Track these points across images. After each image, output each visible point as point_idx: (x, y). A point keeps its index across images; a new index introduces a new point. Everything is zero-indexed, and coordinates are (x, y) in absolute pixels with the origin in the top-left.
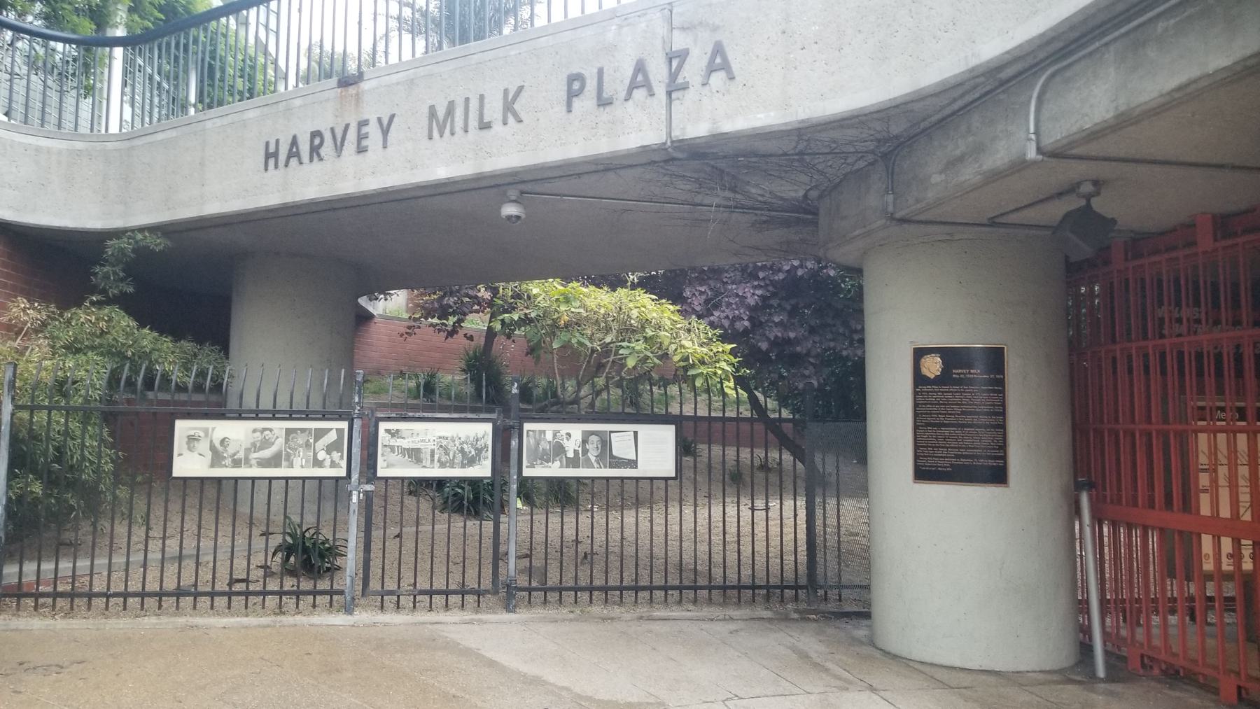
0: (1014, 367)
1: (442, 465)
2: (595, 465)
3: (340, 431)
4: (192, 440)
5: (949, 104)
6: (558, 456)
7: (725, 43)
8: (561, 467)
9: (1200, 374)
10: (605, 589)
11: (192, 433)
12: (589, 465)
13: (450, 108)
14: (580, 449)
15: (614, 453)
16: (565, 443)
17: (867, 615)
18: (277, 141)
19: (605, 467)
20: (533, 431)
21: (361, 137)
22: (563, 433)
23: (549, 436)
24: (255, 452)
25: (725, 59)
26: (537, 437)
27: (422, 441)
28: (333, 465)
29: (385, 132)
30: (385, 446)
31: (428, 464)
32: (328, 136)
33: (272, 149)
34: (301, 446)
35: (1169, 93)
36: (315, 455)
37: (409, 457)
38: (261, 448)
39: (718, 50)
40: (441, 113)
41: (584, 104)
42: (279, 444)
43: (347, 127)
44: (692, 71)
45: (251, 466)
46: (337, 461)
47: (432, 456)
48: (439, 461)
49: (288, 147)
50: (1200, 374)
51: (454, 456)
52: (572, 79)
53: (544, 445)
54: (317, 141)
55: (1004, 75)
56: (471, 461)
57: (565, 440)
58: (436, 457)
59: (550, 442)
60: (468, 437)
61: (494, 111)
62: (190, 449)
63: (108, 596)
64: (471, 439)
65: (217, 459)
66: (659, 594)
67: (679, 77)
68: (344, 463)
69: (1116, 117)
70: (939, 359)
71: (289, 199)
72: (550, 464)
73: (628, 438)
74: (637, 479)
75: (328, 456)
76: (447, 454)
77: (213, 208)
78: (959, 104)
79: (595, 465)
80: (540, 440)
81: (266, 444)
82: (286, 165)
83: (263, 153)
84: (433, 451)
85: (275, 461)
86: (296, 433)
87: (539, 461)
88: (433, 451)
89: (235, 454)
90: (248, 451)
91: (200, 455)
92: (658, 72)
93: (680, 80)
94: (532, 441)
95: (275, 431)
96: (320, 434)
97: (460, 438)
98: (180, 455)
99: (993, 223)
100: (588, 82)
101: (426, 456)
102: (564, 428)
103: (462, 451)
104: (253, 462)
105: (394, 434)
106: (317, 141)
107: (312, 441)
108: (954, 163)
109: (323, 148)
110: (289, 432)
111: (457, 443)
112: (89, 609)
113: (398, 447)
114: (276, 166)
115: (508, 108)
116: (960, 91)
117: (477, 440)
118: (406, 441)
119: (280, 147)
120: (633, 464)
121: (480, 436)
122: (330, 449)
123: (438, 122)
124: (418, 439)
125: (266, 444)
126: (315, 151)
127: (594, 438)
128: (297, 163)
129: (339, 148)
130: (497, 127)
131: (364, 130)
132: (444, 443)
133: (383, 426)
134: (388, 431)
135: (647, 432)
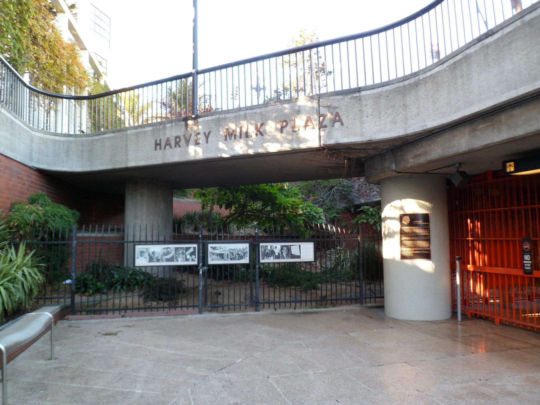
0: (432, 220)
1: (231, 259)
3: (194, 248)
4: (142, 253)
7: (340, 113)
8: (274, 259)
9: (506, 219)
11: (142, 250)
12: (283, 258)
15: (292, 253)
16: (275, 250)
22: (274, 246)
23: (269, 248)
28: (193, 260)
29: (207, 137)
31: (226, 259)
32: (182, 138)
34: (180, 254)
35: (484, 146)
36: (186, 257)
38: (167, 255)
42: (173, 253)
46: (194, 259)
47: (228, 256)
48: (230, 258)
49: (165, 142)
50: (506, 219)
51: (235, 256)
53: (267, 251)
54: (178, 140)
55: (434, 132)
56: (241, 258)
60: (240, 249)
62: (141, 256)
65: (151, 259)
68: (196, 260)
69: (469, 150)
74: (300, 262)
76: (233, 255)
81: (168, 253)
82: (165, 148)
83: (154, 143)
84: (228, 254)
85: (171, 260)
88: (228, 254)
90: (162, 256)
93: (324, 124)
94: (263, 250)
96: (188, 249)
99: (427, 173)
101: (225, 256)
102: (274, 245)
103: (238, 254)
104: (164, 260)
106: (178, 140)
107: (184, 252)
110: (176, 249)
111: (236, 251)
114: (160, 149)
116: (420, 135)
120: (299, 257)
122: (191, 254)
125: (168, 253)
126: (177, 144)
132: (232, 251)
133: (210, 246)
134: (211, 247)
135: (304, 245)
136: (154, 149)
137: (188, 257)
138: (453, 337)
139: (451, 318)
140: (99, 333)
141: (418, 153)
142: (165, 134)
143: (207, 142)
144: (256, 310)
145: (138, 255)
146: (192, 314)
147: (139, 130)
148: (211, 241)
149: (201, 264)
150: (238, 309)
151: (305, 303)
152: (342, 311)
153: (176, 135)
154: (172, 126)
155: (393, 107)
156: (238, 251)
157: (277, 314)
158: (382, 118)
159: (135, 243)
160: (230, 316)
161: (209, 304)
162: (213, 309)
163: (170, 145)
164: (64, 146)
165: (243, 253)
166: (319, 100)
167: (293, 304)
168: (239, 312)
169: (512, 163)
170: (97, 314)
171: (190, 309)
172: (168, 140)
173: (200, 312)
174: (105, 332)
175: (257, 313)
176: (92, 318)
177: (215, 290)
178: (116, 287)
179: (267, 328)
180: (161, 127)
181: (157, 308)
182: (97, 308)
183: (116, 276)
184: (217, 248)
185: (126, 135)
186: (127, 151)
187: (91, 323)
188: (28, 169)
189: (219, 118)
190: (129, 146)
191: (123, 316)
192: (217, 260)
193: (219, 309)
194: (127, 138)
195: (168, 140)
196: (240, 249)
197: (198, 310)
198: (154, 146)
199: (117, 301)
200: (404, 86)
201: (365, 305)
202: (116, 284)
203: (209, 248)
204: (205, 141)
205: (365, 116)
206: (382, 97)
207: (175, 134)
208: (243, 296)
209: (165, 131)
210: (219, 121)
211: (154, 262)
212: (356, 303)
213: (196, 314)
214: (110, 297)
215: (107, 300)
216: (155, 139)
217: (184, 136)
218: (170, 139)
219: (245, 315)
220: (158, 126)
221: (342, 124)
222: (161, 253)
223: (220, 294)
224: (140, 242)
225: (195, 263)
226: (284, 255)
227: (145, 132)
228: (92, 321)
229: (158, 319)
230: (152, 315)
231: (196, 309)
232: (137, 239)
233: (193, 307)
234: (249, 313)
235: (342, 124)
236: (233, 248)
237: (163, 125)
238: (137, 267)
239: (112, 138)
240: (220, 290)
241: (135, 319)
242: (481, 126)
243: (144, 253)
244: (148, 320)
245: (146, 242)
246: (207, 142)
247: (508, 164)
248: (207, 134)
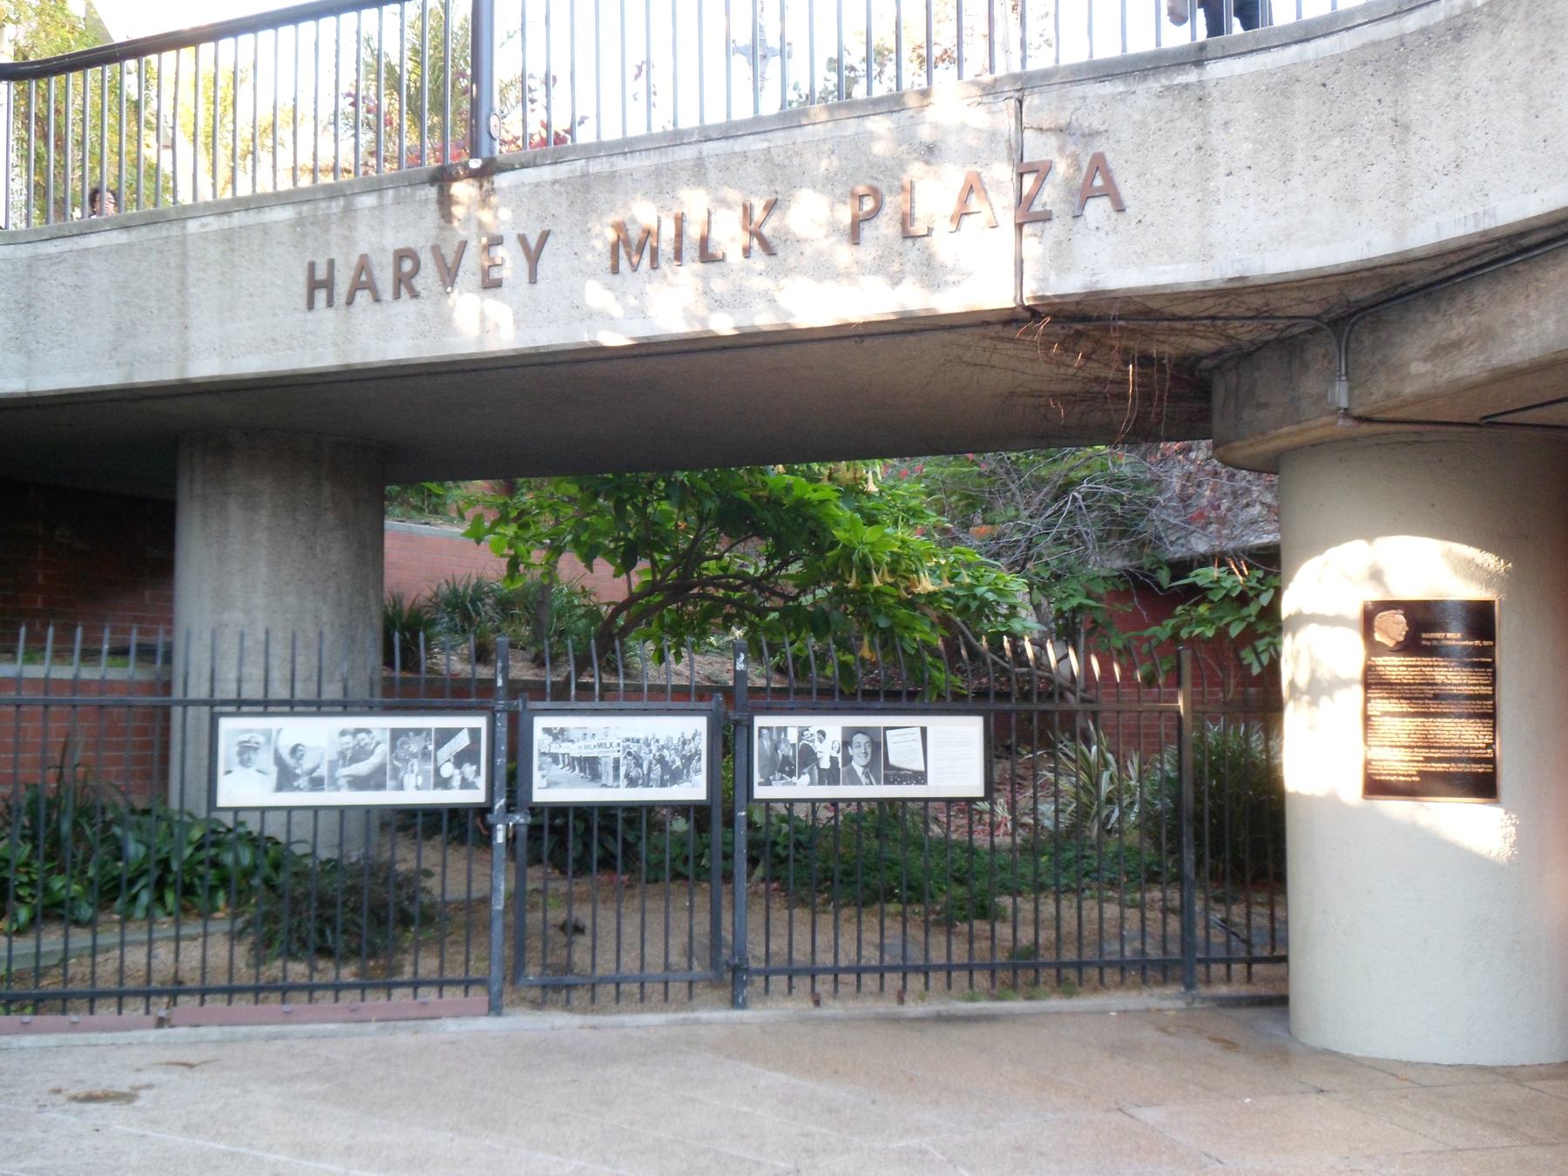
1: (632, 782)
2: (863, 779)
3: (474, 733)
4: (246, 751)
5: (1442, 269)
6: (806, 766)
7: (1109, 157)
8: (812, 783)
11: (245, 737)
12: (853, 779)
14: (840, 756)
15: (893, 761)
16: (817, 747)
18: (331, 263)
19: (878, 783)
20: (768, 728)
22: (814, 730)
23: (792, 736)
24: (344, 766)
25: (1109, 180)
26: (775, 736)
27: (600, 745)
28: (466, 784)
29: (533, 257)
30: (544, 754)
31: (610, 781)
32: (426, 259)
33: (321, 274)
34: (414, 756)
36: (437, 771)
37: (581, 771)
39: (1099, 164)
42: (381, 753)
43: (464, 245)
45: (338, 788)
47: (616, 768)
48: (627, 776)
49: (352, 273)
53: (784, 750)
54: (407, 266)
55: (1525, 242)
56: (673, 776)
57: (817, 743)
58: (622, 771)
59: (793, 746)
60: (670, 739)
62: (244, 763)
64: (675, 741)
65: (286, 779)
67: (1036, 202)
68: (481, 782)
70: (1402, 618)
72: (795, 779)
73: (913, 737)
74: (927, 800)
75: (457, 772)
77: (206, 367)
78: (1458, 269)
79: (863, 779)
80: (779, 742)
81: (359, 754)
82: (350, 301)
83: (301, 278)
84: (617, 761)
85: (374, 781)
86: (408, 736)
87: (778, 775)
88: (617, 761)
89: (314, 770)
90: (333, 766)
91: (260, 771)
94: (767, 744)
95: (375, 733)
96: (445, 736)
97: (657, 741)
98: (228, 772)
99: (1489, 422)
101: (606, 769)
102: (815, 723)
103: (661, 760)
104: (343, 782)
105: (557, 735)
106: (407, 266)
107: (431, 748)
108: (1443, 350)
109: (418, 278)
110: (396, 734)
111: (654, 748)
113: (564, 755)
114: (330, 303)
117: (684, 743)
118: (576, 745)
119: (336, 273)
120: (920, 777)
121: (688, 736)
122: (461, 759)
124: (595, 742)
125: (359, 754)
126: (404, 283)
127: (860, 739)
128: (370, 299)
129: (449, 274)
132: (634, 748)
133: (540, 723)
134: (547, 731)
136: (303, 302)
137: (447, 770)
140: (58, 1091)
142: (349, 241)
143: (533, 278)
144: (735, 1003)
145: (228, 761)
146: (457, 1016)
147: (239, 219)
148: (547, 704)
149: (500, 803)
152: (1104, 1012)
153: (401, 245)
154: (381, 206)
155: (1348, 129)
157: (822, 1021)
158: (1296, 182)
159: (217, 709)
160: (622, 1026)
161: (532, 972)
162: (550, 995)
163: (371, 286)
165: (683, 757)
166: (1021, 102)
167: (893, 980)
168: (662, 1010)
170: (50, 1010)
171: (453, 994)
172: (364, 265)
173: (495, 1009)
174: (80, 1090)
175: (737, 1014)
176: (25, 1029)
177: (557, 915)
178: (135, 898)
179: (781, 1077)
180: (336, 206)
181: (310, 989)
182: (49, 984)
183: (134, 849)
185: (183, 242)
186: (183, 312)
187: (21, 1049)
189: (585, 175)
190: (193, 290)
191: (161, 1023)
192: (572, 784)
193: (575, 994)
194: (185, 254)
195: (364, 265)
197: (486, 999)
198: (301, 289)
199: (136, 957)
200: (1401, 40)
201: (1203, 991)
202: (132, 882)
205: (1222, 170)
206: (1298, 87)
207: (394, 240)
208: (678, 941)
209: (351, 229)
210: (587, 188)
211: (298, 788)
212: (1165, 981)
213: (476, 1015)
214: (108, 937)
215: (94, 951)
216: (310, 259)
217: (436, 250)
218: (374, 260)
219: (685, 1022)
220: (322, 205)
222: (332, 754)
223: (579, 930)
224: (241, 706)
225: (478, 796)
226: (858, 766)
227: (265, 229)
228: (27, 1041)
229: (311, 1037)
230: (287, 1018)
231: (478, 996)
232: (227, 690)
233: (467, 984)
234: (704, 1015)
236: (641, 736)
237: (342, 202)
239: (119, 249)
240: (582, 913)
241: (214, 1032)
243: (256, 749)
244: (269, 1038)
245: (266, 706)
246: (533, 278)
248: (533, 242)
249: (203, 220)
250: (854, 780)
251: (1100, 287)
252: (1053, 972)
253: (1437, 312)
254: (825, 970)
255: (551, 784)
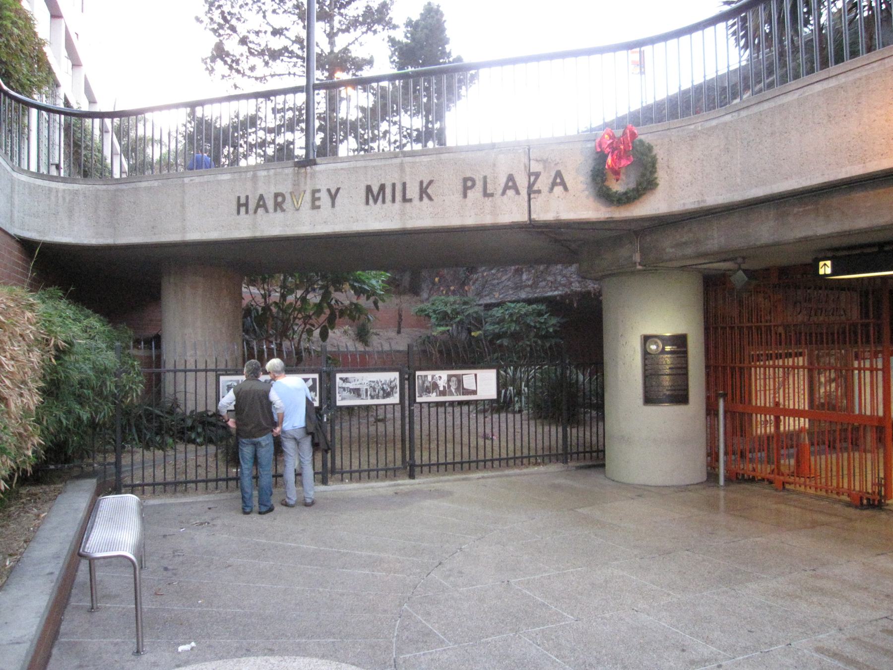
1: (372, 397)
3: (314, 380)
7: (563, 172)
8: (437, 396)
10: (438, 465)
11: (230, 383)
12: (451, 394)
13: (382, 188)
15: (465, 386)
17: (603, 466)
18: (247, 197)
21: (314, 199)
22: (437, 376)
23: (430, 379)
29: (333, 197)
32: (288, 196)
33: (243, 201)
39: (559, 174)
40: (375, 189)
41: (475, 194)
44: (543, 183)
47: (367, 392)
48: (370, 395)
52: (465, 180)
53: (427, 384)
56: (387, 395)
60: (386, 381)
61: (413, 192)
63: (469, 462)
66: (381, 473)
71: (258, 234)
74: (477, 401)
82: (255, 212)
83: (235, 203)
84: (367, 390)
92: (522, 182)
93: (535, 188)
94: (420, 382)
100: (477, 182)
101: (363, 393)
102: (438, 373)
103: (383, 389)
105: (345, 380)
106: (280, 199)
111: (380, 384)
112: (446, 470)
114: (247, 212)
115: (424, 192)
120: (474, 392)
123: (373, 196)
126: (278, 206)
127: (454, 379)
130: (416, 202)
131: (317, 195)
132: (373, 384)
133: (338, 376)
134: (341, 379)
136: (235, 212)
138: (712, 505)
139: (707, 480)
141: (683, 240)
143: (333, 205)
149: (325, 407)
150: (519, 463)
151: (459, 466)
156: (382, 385)
159: (218, 373)
164: (64, 199)
165: (390, 387)
169: (829, 263)
172: (261, 197)
175: (412, 481)
184: (350, 380)
188: (8, 239)
192: (350, 399)
195: (261, 197)
196: (386, 381)
198: (235, 207)
203: (338, 380)
204: (330, 204)
207: (273, 190)
218: (265, 196)
219: (395, 485)
221: (566, 189)
234: (400, 482)
235: (566, 189)
236: (375, 379)
238: (499, 393)
242: (796, 210)
246: (333, 205)
247: (821, 263)
248: (333, 192)
249: (192, 178)
250: (452, 394)
251: (559, 218)
252: (444, 466)
253: (677, 231)
254: (347, 472)
255: (343, 399)
